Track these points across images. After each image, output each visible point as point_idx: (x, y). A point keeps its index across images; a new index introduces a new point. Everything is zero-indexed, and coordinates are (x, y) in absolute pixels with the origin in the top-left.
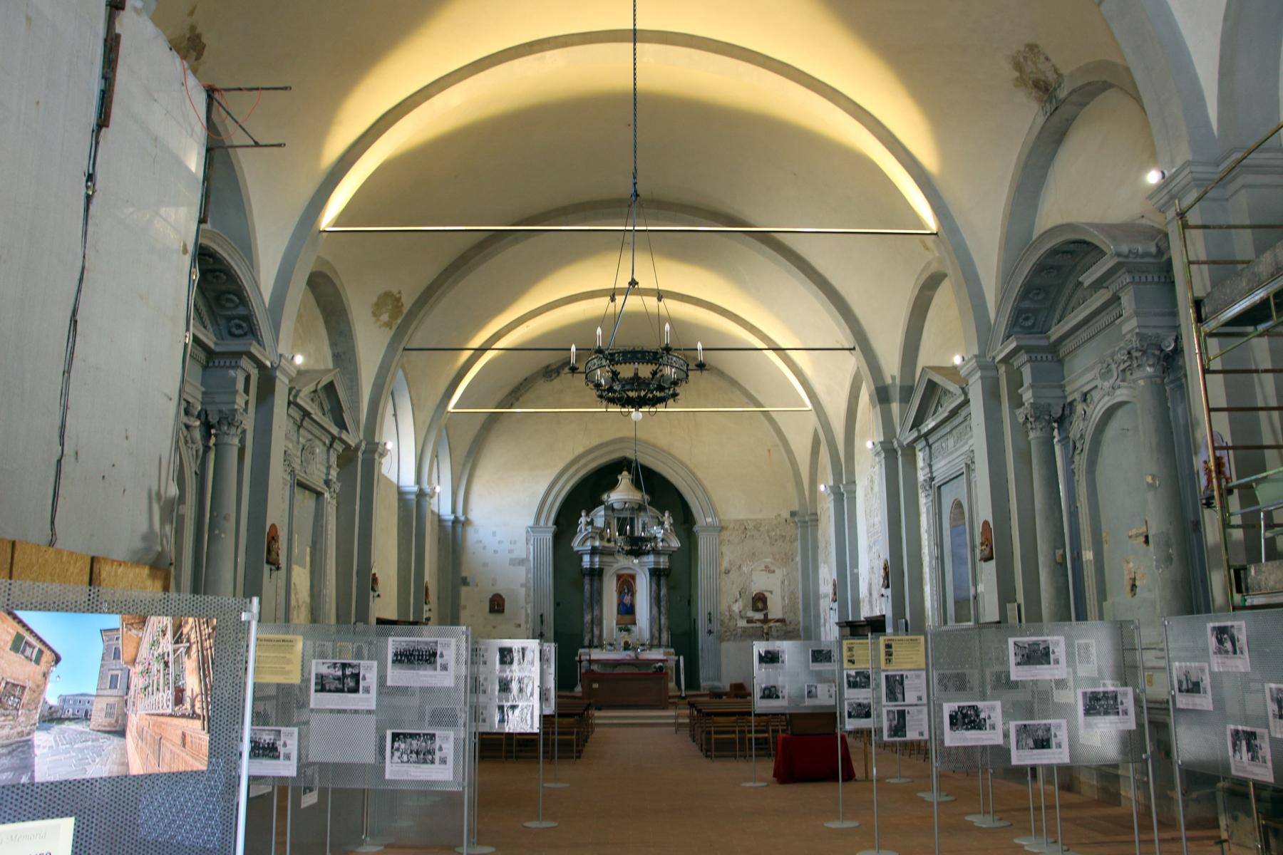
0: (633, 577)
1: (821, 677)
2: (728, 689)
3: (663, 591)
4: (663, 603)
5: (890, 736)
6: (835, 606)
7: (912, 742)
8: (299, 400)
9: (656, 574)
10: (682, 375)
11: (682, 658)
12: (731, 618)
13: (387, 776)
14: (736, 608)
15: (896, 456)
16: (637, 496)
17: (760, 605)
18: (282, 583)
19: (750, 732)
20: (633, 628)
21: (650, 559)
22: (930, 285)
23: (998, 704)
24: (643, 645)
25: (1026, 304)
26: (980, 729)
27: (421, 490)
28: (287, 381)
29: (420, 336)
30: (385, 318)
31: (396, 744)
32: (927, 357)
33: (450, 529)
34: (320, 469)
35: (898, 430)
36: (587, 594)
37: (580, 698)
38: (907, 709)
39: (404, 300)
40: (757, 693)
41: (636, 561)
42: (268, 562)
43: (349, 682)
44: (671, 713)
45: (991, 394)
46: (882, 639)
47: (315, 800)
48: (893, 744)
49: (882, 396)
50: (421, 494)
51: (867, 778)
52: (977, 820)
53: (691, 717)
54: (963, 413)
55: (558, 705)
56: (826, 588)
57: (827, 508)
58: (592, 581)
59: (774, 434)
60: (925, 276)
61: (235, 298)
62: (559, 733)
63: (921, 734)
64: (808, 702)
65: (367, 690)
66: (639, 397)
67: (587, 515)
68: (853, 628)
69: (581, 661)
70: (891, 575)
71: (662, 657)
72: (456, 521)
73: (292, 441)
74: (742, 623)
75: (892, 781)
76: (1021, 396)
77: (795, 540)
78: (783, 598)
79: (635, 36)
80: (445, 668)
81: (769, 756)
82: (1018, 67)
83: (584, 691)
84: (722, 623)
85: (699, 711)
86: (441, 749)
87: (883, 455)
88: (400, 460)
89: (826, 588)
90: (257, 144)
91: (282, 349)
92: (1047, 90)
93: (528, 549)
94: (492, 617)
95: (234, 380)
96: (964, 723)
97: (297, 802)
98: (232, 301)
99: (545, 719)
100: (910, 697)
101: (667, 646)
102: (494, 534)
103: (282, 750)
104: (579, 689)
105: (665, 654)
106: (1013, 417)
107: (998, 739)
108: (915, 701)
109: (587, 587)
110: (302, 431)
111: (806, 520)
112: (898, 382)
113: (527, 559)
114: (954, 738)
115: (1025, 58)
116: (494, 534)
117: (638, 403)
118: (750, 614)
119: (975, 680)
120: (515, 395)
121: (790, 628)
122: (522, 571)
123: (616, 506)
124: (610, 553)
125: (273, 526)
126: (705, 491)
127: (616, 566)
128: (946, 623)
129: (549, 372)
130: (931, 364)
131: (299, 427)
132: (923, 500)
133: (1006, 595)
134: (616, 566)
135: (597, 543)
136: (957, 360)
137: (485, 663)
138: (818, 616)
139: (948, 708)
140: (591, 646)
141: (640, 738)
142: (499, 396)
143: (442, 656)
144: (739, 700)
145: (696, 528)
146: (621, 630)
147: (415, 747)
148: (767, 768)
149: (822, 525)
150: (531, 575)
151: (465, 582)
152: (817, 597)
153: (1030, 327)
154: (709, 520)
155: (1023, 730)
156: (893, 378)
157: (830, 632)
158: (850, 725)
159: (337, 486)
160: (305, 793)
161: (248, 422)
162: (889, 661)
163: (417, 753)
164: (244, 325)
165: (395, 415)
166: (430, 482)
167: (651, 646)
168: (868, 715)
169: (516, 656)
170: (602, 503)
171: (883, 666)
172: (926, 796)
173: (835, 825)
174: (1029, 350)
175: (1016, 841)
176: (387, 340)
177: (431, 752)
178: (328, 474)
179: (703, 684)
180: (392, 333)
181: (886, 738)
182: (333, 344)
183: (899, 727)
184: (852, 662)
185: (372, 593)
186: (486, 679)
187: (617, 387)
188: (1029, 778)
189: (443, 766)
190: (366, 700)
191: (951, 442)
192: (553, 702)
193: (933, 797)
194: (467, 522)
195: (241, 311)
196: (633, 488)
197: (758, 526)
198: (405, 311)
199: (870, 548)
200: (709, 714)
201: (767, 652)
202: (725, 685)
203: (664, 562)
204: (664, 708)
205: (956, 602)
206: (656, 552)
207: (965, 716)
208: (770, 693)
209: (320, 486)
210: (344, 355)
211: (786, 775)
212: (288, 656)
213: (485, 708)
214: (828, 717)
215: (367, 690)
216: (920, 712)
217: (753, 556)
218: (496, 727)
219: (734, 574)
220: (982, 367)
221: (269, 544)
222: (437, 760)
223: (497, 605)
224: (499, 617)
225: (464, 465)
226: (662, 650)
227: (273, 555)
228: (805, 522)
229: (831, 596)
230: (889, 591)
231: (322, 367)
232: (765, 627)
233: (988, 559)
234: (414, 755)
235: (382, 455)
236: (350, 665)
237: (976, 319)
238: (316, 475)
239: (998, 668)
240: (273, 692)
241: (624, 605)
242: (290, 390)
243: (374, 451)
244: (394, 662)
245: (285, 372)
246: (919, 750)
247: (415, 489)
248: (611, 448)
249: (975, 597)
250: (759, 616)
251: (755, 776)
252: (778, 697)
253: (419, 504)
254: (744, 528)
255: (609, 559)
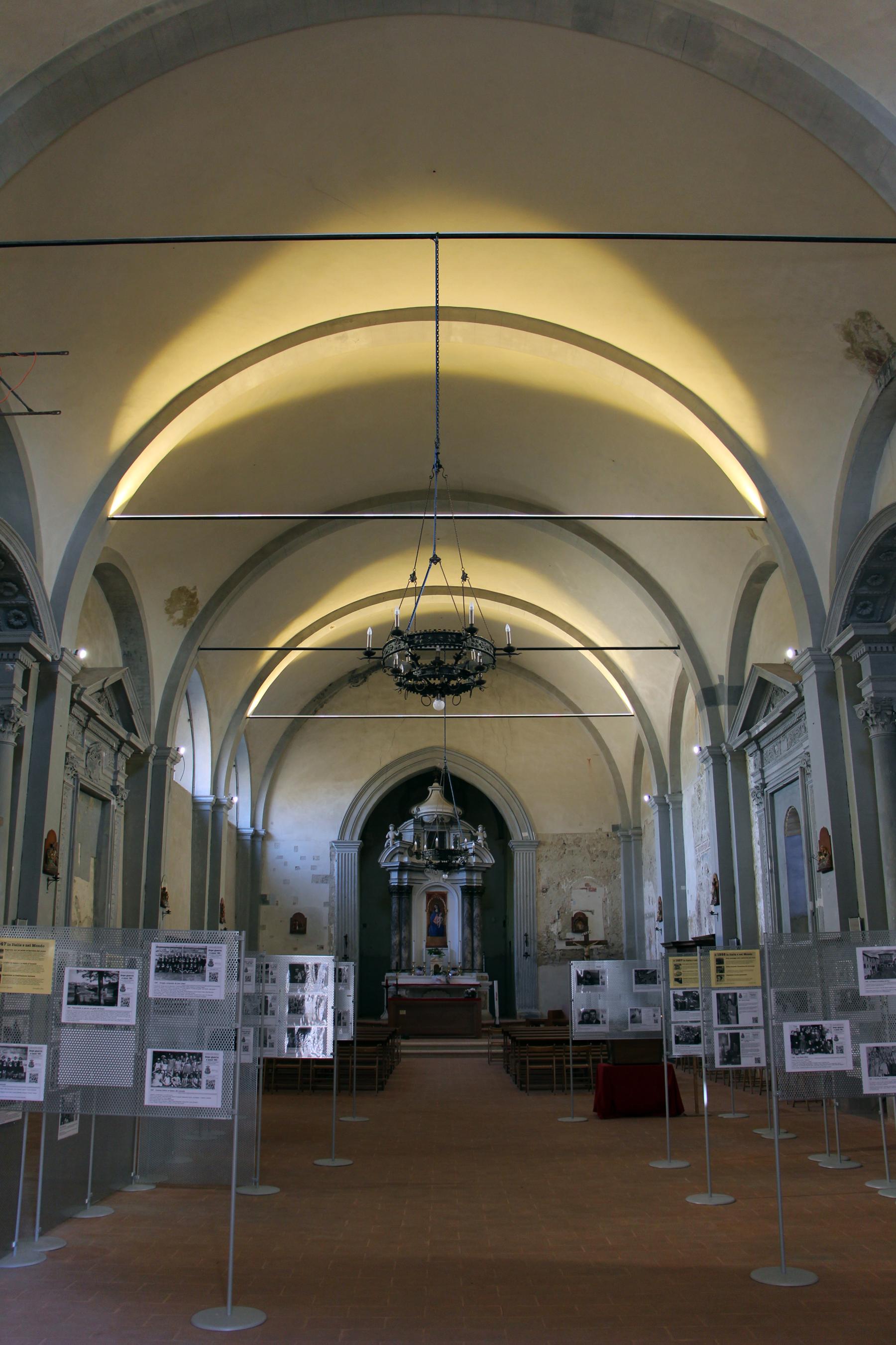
0: (444, 896)
1: (644, 999)
2: (546, 1016)
3: (476, 911)
4: (476, 924)
5: (722, 1063)
6: (661, 925)
7: (747, 1070)
8: (83, 699)
9: (468, 892)
10: (489, 660)
11: (496, 983)
12: (549, 939)
13: (147, 1102)
14: (555, 929)
15: (724, 762)
16: (448, 809)
17: (580, 926)
18: (61, 896)
19: (568, 1062)
20: (444, 951)
21: (462, 876)
22: (760, 576)
23: (846, 1024)
24: (454, 969)
25: (864, 591)
26: (827, 1052)
27: (255, 831)
28: (70, 679)
29: (216, 635)
30: (179, 615)
31: (158, 1065)
32: (758, 653)
33: (249, 843)
34: (107, 773)
35: (727, 734)
36: (395, 913)
37: (386, 1026)
38: (741, 1032)
39: (199, 596)
40: (575, 1019)
41: (445, 876)
42: (45, 872)
43: (105, 993)
44: (485, 1042)
45: (828, 691)
46: (712, 953)
47: (76, 1131)
48: (726, 1072)
49: (709, 697)
50: (217, 805)
51: (698, 1114)
52: (823, 1160)
53: (504, 1046)
54: (797, 712)
55: (357, 1032)
56: (651, 907)
57: (652, 820)
58: (400, 899)
59: (592, 739)
60: (753, 568)
61: (14, 586)
62: (358, 1063)
63: (758, 1060)
64: (632, 1028)
65: (126, 1003)
66: (442, 685)
67: (395, 829)
68: (679, 947)
69: (387, 986)
70: (722, 891)
71: (474, 982)
72: (255, 835)
73: (75, 743)
74: (561, 946)
75: (725, 1116)
76: (860, 690)
77: (618, 856)
78: (605, 919)
79: (438, 313)
80: (214, 978)
81: (589, 1088)
82: (849, 336)
83: (384, 1017)
84: (540, 945)
85: (513, 1039)
86: (208, 1071)
87: (711, 761)
88: (195, 768)
89: (651, 907)
90: (31, 412)
91: (66, 642)
92: (881, 361)
93: (332, 865)
94: (293, 938)
95: (11, 674)
96: (808, 1046)
97: (52, 1132)
98: (10, 589)
99: (339, 1045)
100: (745, 1019)
101: (481, 971)
102: (296, 848)
103: (28, 1071)
104: (385, 1016)
105: (478, 979)
106: (852, 713)
107: (848, 1066)
108: (750, 1023)
109: (395, 906)
110: (87, 733)
111: (628, 835)
112: (726, 682)
113: (331, 876)
114: (797, 1063)
115: (857, 328)
116: (296, 848)
117: (442, 691)
118: (570, 935)
119: (816, 1000)
120: (321, 699)
121: (612, 951)
122: (326, 887)
123: (426, 819)
124: (420, 870)
125: (52, 833)
126: (521, 804)
127: (426, 884)
128: (781, 943)
129: (356, 677)
130: (761, 662)
131: (84, 728)
132: (754, 809)
133: (848, 908)
134: (426, 884)
135: (406, 860)
136: (790, 654)
137: (274, 981)
138: (642, 938)
139: (789, 1028)
140: (399, 969)
141: (450, 1069)
142: (303, 702)
143: (211, 964)
144: (557, 1027)
145: (511, 843)
146: (430, 952)
147: (179, 1068)
148: (587, 1101)
149: (646, 839)
150: (335, 894)
151: (264, 900)
152: (642, 917)
153: (867, 616)
154: (525, 834)
155: (875, 1054)
156: (721, 678)
157: (655, 950)
158: (678, 1051)
159: (125, 794)
160: (63, 1122)
161: (27, 719)
162: (720, 978)
163: (182, 1076)
164: (24, 615)
165: (190, 720)
166: (227, 792)
167: (464, 970)
168: (697, 1041)
169: (310, 972)
170: (411, 816)
171: (713, 983)
172: (764, 1133)
173: (661, 1165)
174: (868, 639)
175: (868, 1185)
176: (181, 639)
177: (197, 1075)
178: (115, 780)
179: (519, 1011)
180: (186, 632)
181: (717, 1065)
182: (124, 642)
183: (732, 1054)
184: (679, 981)
185: (161, 909)
186: (274, 999)
187: (417, 673)
188: (881, 1111)
189: (210, 1091)
190: (124, 1014)
191: (784, 745)
192: (351, 1027)
193: (772, 1134)
194: (267, 836)
195: (21, 600)
196: (443, 800)
197: (577, 842)
198: (200, 608)
199: (698, 862)
200: (523, 1043)
201: (587, 973)
202: (543, 1012)
203: (477, 879)
204: (477, 1036)
205: (793, 919)
206: (470, 870)
207: (808, 1037)
208: (590, 1017)
209: (107, 793)
210: (135, 653)
211: (610, 1108)
212: (39, 963)
213: (273, 1031)
214: (653, 1044)
215: (126, 1003)
216: (756, 1035)
217: (572, 873)
218: (285, 1052)
219: (552, 892)
220: (817, 661)
221: (46, 851)
222: (204, 1085)
223: (298, 925)
224: (301, 938)
225: (265, 776)
226: (474, 975)
227: (51, 864)
228: (629, 837)
229: (656, 915)
230: (719, 908)
231: (112, 666)
232: (586, 949)
233: (827, 870)
234: (178, 1078)
235: (175, 761)
236: (107, 974)
237: (809, 609)
238: (102, 780)
239: (844, 986)
240: (26, 1005)
241: (435, 925)
242: (74, 687)
243: (166, 757)
244: (157, 970)
245: (68, 668)
246: (753, 1080)
247: (211, 799)
248: (420, 758)
249: (814, 913)
250: (579, 937)
251: (573, 1110)
252: (598, 1022)
253: (214, 814)
254: (562, 843)
255: (416, 876)
